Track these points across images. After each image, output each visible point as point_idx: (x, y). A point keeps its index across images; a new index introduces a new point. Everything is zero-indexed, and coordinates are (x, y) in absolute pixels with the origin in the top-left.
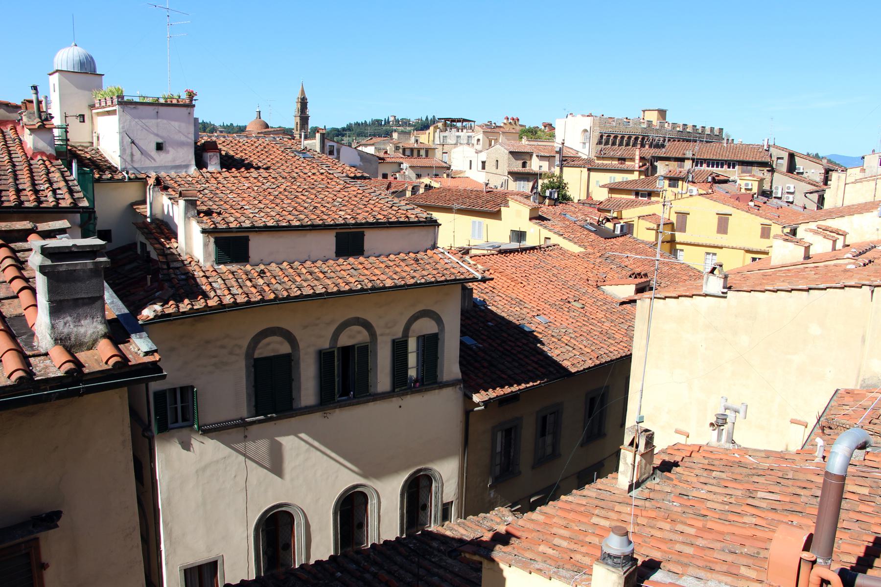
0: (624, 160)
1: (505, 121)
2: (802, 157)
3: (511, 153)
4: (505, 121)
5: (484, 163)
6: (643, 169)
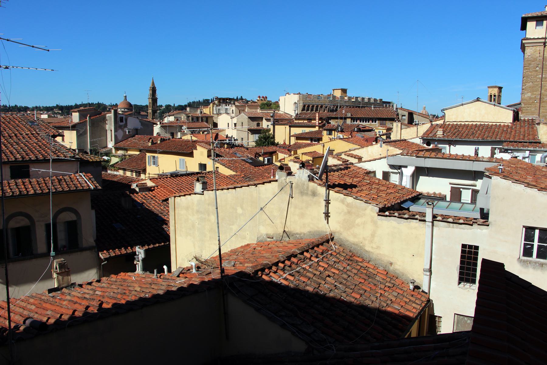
0: (311, 120)
1: (258, 99)
2: (420, 115)
3: (249, 118)
4: (258, 99)
5: (235, 124)
6: (320, 125)
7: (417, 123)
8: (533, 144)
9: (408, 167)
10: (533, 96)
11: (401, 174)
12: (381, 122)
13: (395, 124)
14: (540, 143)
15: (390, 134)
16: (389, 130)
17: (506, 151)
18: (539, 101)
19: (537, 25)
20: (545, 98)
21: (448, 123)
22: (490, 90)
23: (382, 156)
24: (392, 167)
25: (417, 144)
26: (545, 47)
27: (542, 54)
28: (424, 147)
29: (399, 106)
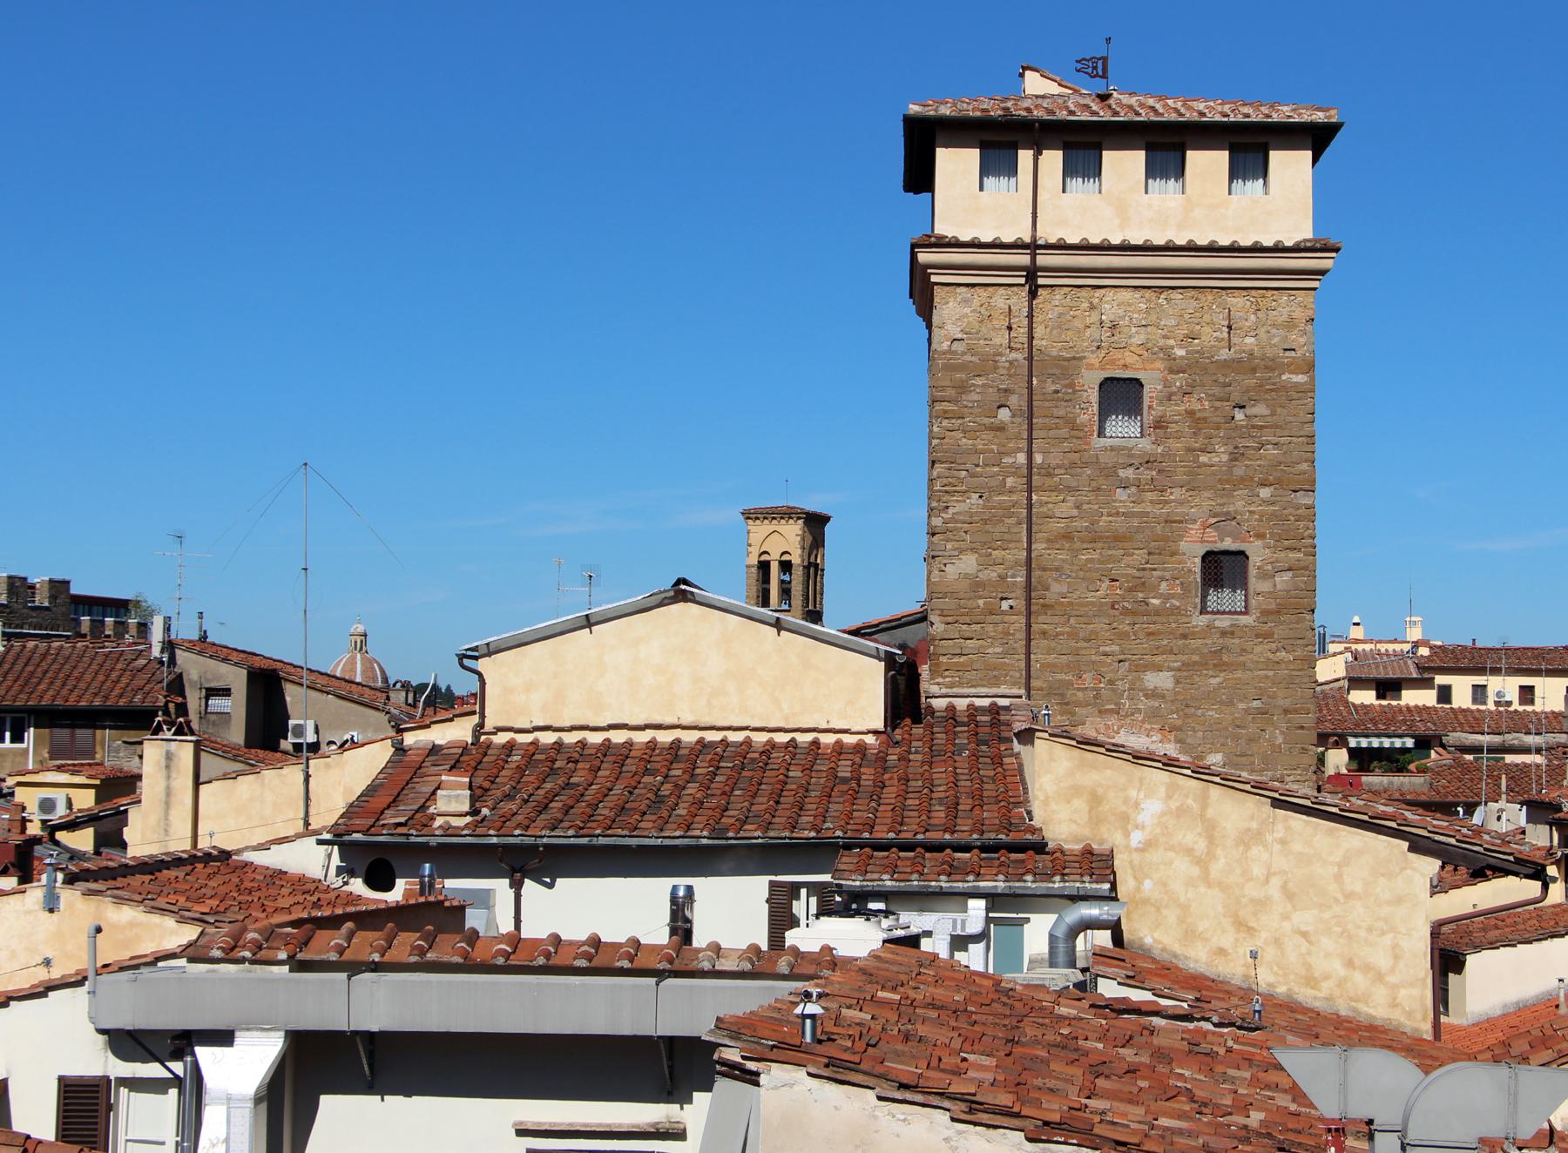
2: (325, 683)
7: (311, 737)
8: (1003, 856)
9: (241, 1038)
10: (992, 574)
11: (193, 1091)
12: (63, 734)
13: (153, 751)
14: (1040, 848)
15: (121, 817)
16: (119, 787)
17: (852, 904)
18: (1020, 604)
19: (985, 170)
20: (1057, 588)
21: (501, 739)
22: (760, 530)
23: (56, 973)
24: (125, 1042)
25: (301, 880)
26: (1033, 294)
27: (1021, 333)
28: (354, 899)
29: (186, 630)
